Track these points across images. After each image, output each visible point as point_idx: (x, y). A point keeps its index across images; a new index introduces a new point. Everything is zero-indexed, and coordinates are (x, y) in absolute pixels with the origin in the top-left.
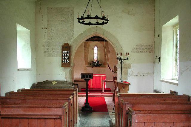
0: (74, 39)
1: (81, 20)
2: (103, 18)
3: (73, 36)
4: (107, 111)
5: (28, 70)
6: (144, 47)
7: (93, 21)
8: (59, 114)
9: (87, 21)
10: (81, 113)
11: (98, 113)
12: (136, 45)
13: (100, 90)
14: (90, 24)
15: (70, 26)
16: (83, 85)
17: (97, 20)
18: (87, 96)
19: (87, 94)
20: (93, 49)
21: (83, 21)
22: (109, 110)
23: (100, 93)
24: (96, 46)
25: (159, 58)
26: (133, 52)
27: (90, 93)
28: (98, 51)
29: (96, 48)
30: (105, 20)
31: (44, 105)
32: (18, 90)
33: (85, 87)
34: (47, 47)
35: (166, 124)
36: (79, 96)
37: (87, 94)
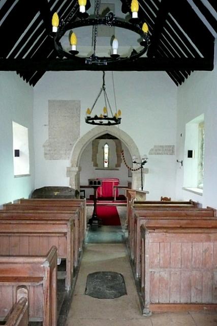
0: (80, 138)
1: (89, 120)
2: (114, 119)
3: (79, 134)
4: (120, 224)
5: (26, 175)
6: (164, 149)
7: (106, 122)
8: (64, 231)
9: (96, 121)
10: (89, 226)
11: (108, 226)
12: (155, 146)
13: (111, 199)
14: (101, 124)
15: (76, 122)
16: (90, 192)
17: (107, 132)
18: (95, 205)
19: (95, 203)
20: (103, 148)
21: (93, 122)
22: (122, 222)
23: (111, 201)
24: (106, 143)
25: (182, 162)
26: (151, 154)
27: (100, 201)
28: (109, 150)
29: (106, 146)
30: (117, 121)
31: (43, 312)
32: (14, 201)
33: (93, 194)
34: (48, 148)
35: (169, 150)
36: (87, 205)
37: (95, 203)
